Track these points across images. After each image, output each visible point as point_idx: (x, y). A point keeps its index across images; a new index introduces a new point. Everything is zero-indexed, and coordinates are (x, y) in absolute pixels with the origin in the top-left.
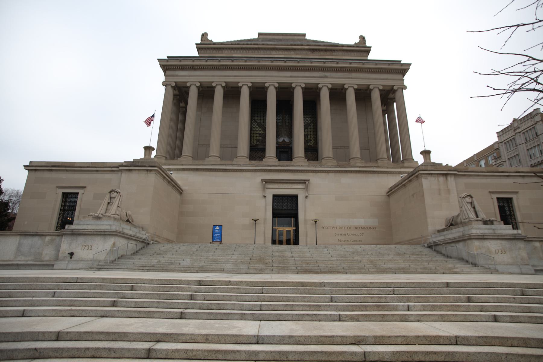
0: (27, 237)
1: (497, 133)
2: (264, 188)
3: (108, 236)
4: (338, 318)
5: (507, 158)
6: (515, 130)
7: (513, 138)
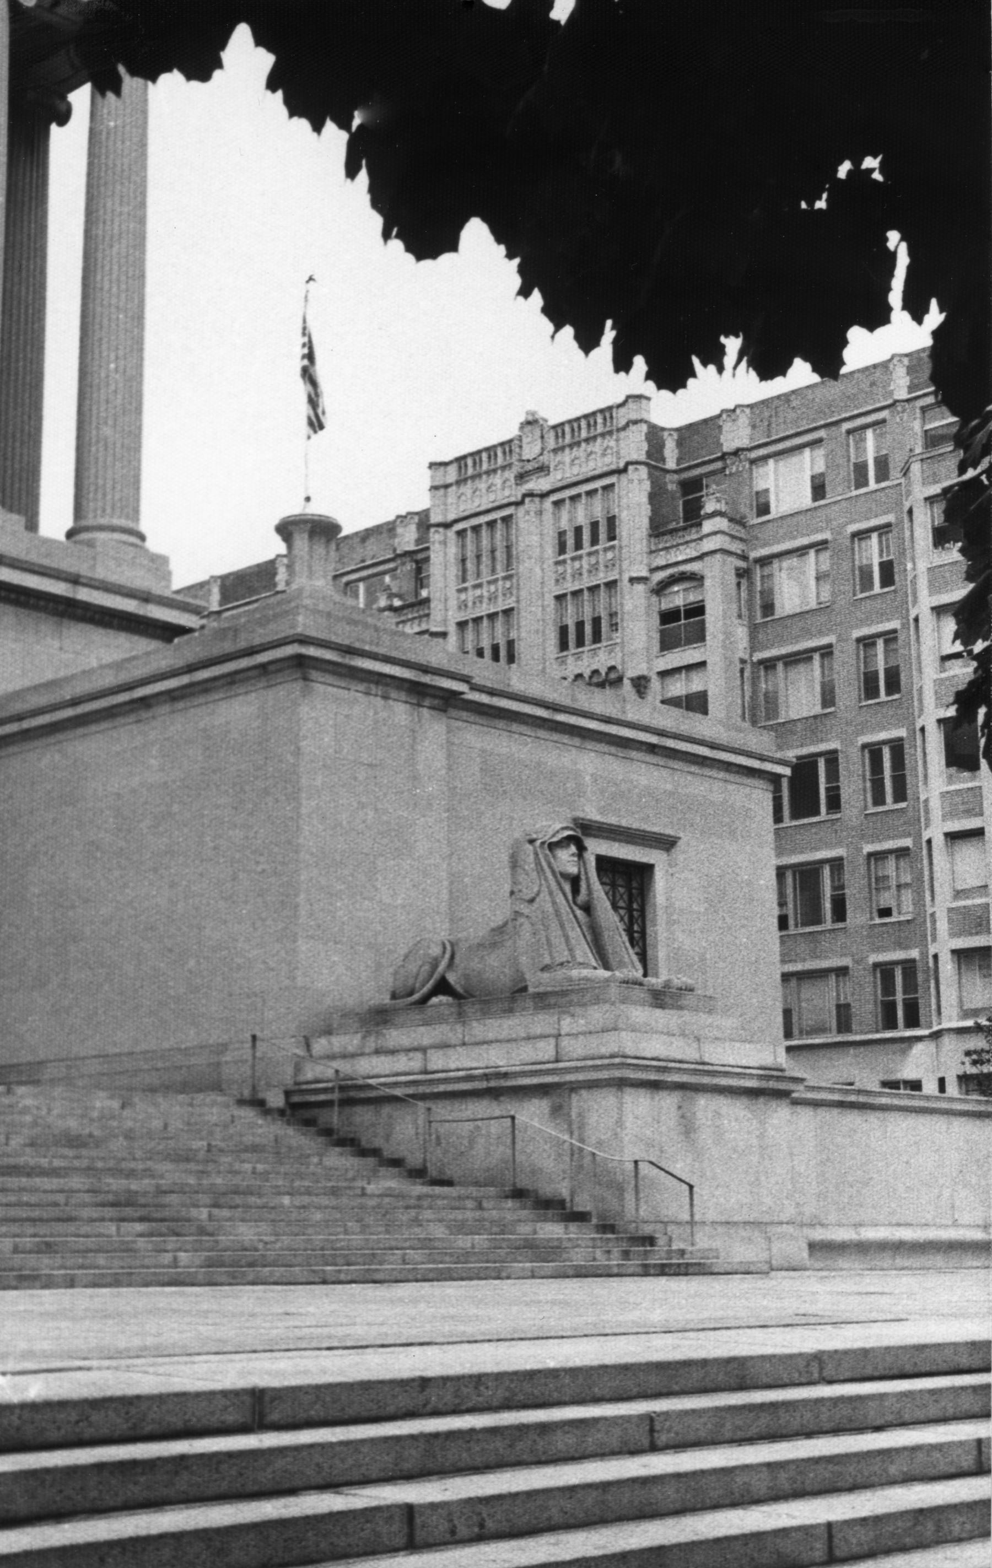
1: (432, 465)
4: (397, 1526)
5: (455, 616)
6: (521, 477)
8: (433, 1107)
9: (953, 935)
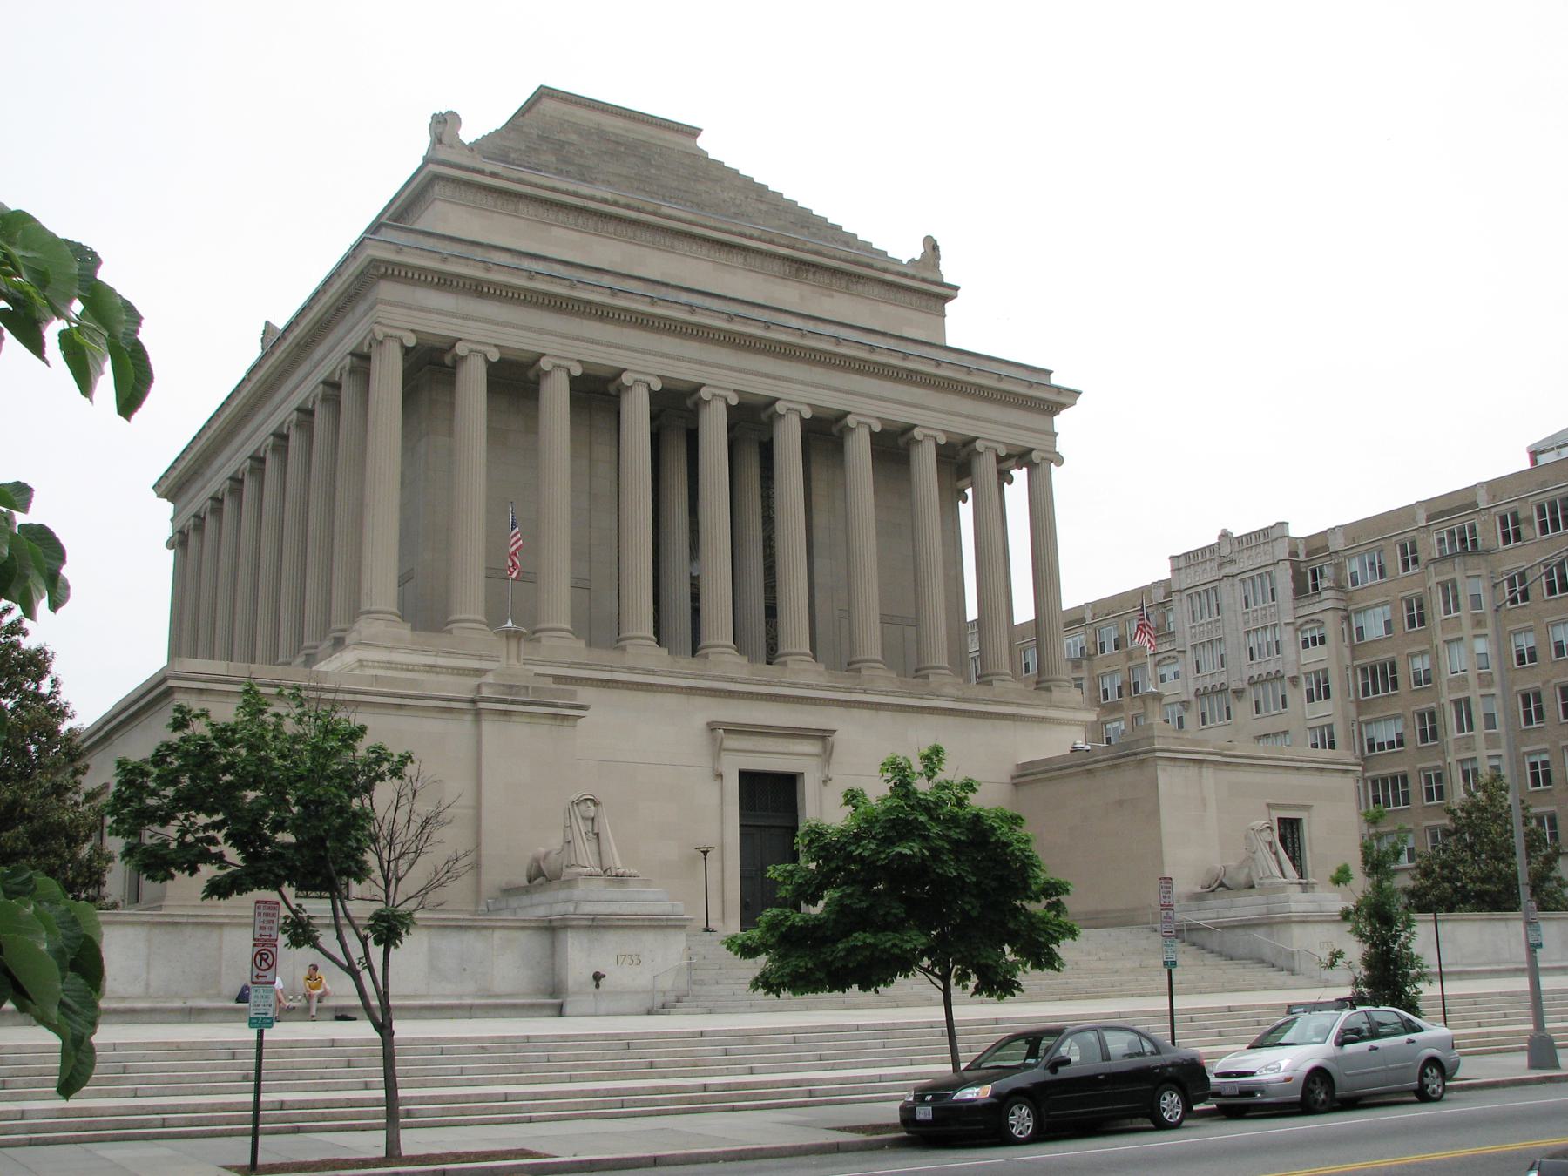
0: (448, 931)
1: (1172, 558)
2: (718, 750)
3: (673, 931)
6: (1221, 565)
7: (1215, 589)
8: (1182, 960)
9: (1456, 751)
